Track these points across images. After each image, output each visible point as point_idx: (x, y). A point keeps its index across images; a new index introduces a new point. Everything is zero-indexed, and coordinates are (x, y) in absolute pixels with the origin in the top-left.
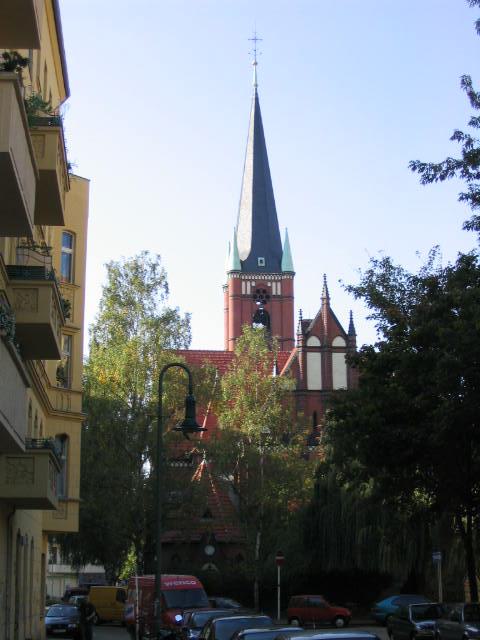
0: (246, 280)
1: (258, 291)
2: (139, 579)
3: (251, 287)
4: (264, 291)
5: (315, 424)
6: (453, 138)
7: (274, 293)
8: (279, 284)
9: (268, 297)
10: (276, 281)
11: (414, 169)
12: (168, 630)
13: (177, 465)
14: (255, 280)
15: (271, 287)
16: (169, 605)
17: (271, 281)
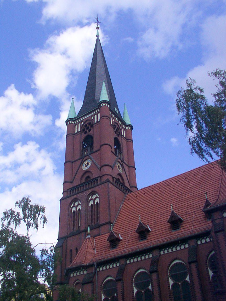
4: (90, 124)
7: (96, 122)
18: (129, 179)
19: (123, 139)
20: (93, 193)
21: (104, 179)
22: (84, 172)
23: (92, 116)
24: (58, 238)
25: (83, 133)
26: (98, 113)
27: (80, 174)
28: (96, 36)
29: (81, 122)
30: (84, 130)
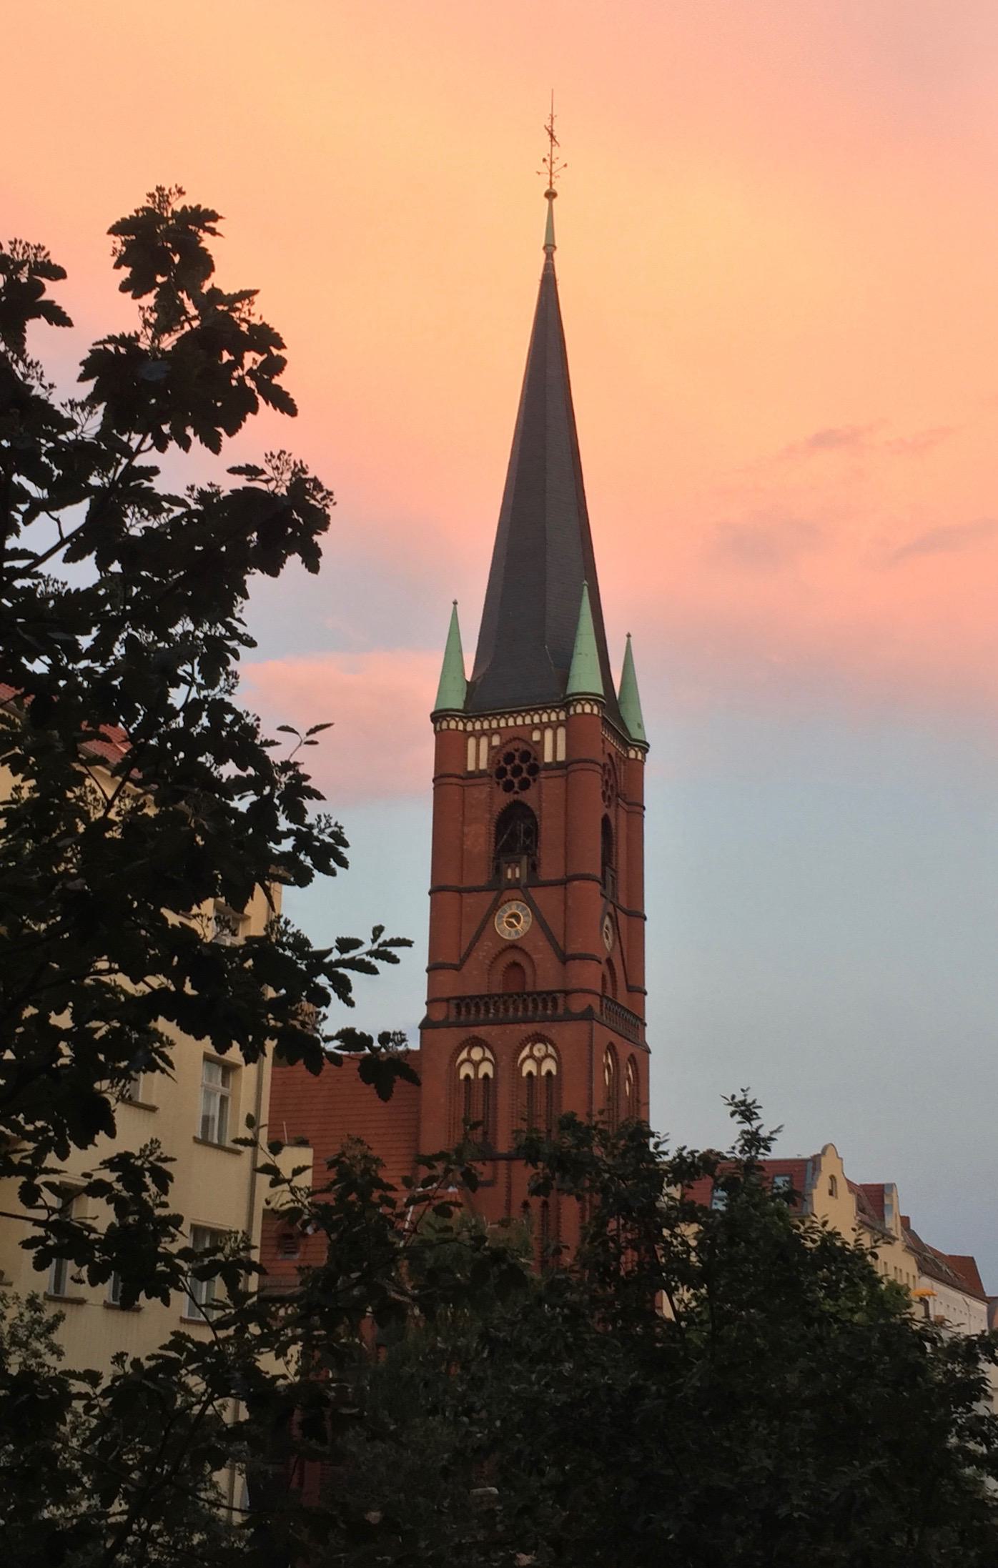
0: (478, 735)
1: (509, 758)
2: (181, 1356)
3: (491, 747)
4: (526, 756)
5: (281, 1286)
6: (184, 193)
7: (548, 758)
8: (561, 732)
9: (534, 770)
10: (554, 726)
11: (37, 363)
12: (198, 636)
13: (519, 721)
14: (497, 731)
15: (541, 743)
16: (128, 784)
17: (542, 727)
18: (625, 953)
19: (620, 809)
20: (538, 1038)
21: (578, 1004)
22: (503, 946)
23: (535, 727)
24: (192, 1037)
25: (498, 784)
26: (559, 724)
27: (484, 950)
28: (545, 248)
29: (489, 733)
30: (501, 773)
